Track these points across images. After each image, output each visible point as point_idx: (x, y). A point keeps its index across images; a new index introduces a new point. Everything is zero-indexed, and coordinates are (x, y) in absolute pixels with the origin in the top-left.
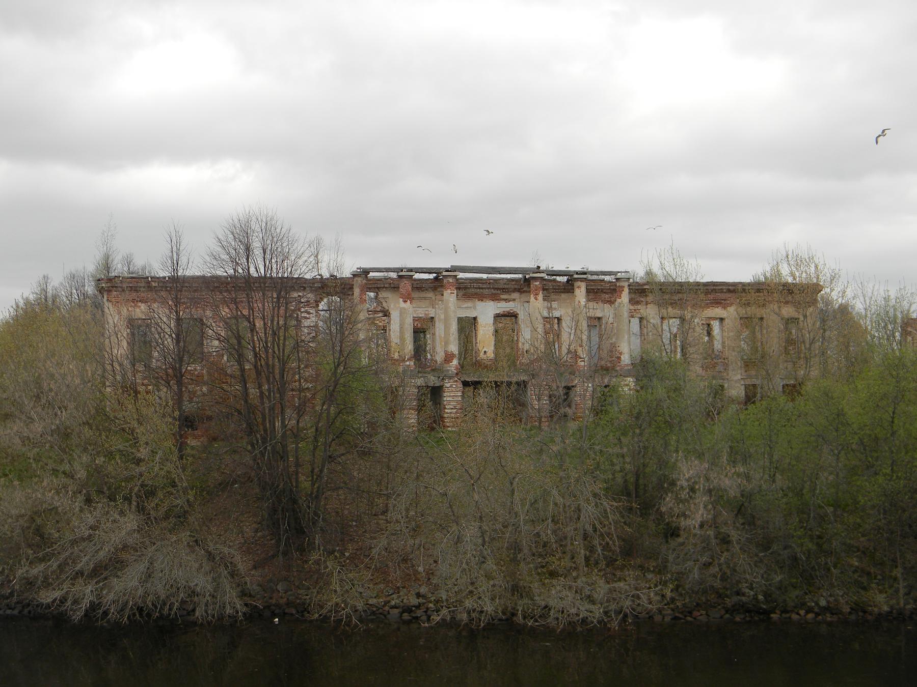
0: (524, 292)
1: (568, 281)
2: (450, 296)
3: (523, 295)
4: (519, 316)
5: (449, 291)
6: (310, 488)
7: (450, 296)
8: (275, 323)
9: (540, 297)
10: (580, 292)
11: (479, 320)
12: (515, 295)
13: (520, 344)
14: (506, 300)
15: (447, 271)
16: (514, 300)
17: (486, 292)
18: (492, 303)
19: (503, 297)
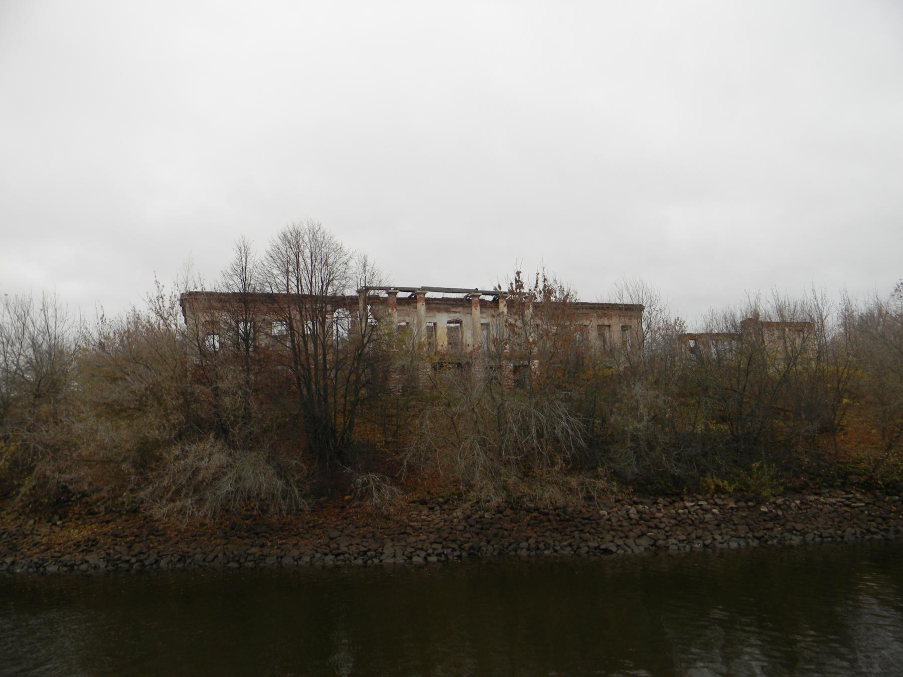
0: (466, 307)
1: (494, 299)
2: (476, 311)
3: (466, 309)
4: (463, 322)
5: (421, 303)
6: (844, 343)
7: (476, 311)
8: (297, 350)
9: (479, 308)
10: (421, 307)
11: (438, 325)
12: (460, 309)
13: (464, 340)
14: (455, 312)
15: (419, 289)
16: (459, 312)
17: (442, 306)
18: (446, 314)
19: (452, 310)
